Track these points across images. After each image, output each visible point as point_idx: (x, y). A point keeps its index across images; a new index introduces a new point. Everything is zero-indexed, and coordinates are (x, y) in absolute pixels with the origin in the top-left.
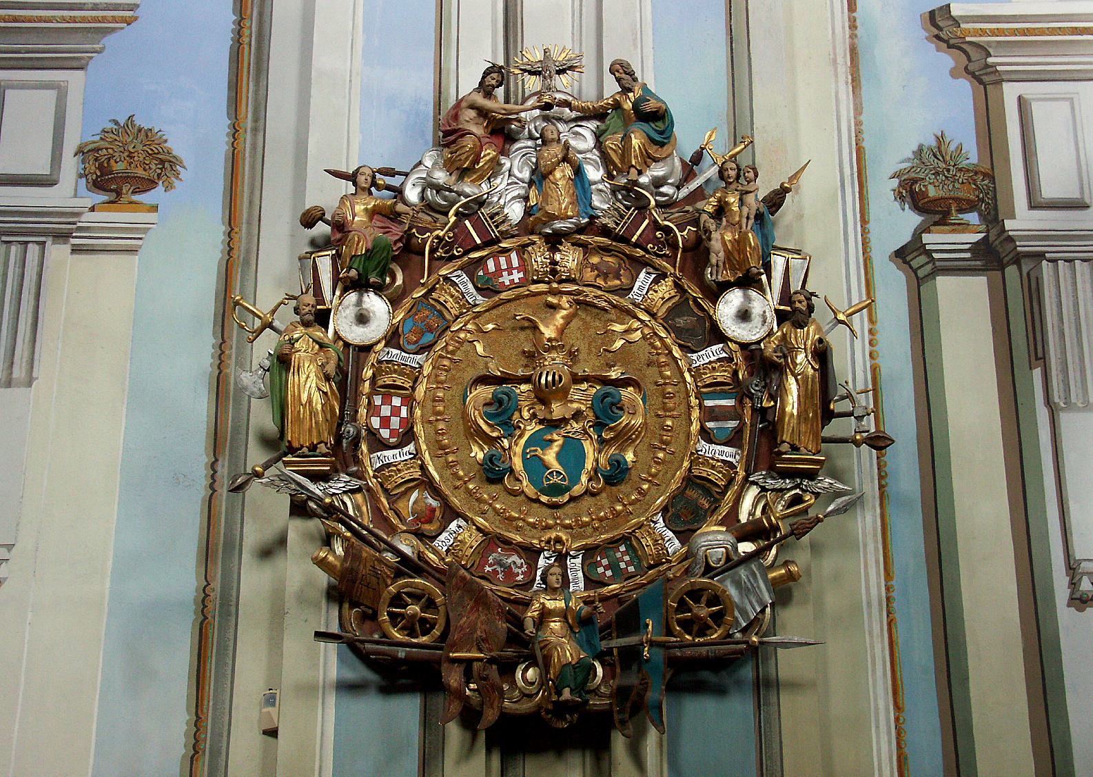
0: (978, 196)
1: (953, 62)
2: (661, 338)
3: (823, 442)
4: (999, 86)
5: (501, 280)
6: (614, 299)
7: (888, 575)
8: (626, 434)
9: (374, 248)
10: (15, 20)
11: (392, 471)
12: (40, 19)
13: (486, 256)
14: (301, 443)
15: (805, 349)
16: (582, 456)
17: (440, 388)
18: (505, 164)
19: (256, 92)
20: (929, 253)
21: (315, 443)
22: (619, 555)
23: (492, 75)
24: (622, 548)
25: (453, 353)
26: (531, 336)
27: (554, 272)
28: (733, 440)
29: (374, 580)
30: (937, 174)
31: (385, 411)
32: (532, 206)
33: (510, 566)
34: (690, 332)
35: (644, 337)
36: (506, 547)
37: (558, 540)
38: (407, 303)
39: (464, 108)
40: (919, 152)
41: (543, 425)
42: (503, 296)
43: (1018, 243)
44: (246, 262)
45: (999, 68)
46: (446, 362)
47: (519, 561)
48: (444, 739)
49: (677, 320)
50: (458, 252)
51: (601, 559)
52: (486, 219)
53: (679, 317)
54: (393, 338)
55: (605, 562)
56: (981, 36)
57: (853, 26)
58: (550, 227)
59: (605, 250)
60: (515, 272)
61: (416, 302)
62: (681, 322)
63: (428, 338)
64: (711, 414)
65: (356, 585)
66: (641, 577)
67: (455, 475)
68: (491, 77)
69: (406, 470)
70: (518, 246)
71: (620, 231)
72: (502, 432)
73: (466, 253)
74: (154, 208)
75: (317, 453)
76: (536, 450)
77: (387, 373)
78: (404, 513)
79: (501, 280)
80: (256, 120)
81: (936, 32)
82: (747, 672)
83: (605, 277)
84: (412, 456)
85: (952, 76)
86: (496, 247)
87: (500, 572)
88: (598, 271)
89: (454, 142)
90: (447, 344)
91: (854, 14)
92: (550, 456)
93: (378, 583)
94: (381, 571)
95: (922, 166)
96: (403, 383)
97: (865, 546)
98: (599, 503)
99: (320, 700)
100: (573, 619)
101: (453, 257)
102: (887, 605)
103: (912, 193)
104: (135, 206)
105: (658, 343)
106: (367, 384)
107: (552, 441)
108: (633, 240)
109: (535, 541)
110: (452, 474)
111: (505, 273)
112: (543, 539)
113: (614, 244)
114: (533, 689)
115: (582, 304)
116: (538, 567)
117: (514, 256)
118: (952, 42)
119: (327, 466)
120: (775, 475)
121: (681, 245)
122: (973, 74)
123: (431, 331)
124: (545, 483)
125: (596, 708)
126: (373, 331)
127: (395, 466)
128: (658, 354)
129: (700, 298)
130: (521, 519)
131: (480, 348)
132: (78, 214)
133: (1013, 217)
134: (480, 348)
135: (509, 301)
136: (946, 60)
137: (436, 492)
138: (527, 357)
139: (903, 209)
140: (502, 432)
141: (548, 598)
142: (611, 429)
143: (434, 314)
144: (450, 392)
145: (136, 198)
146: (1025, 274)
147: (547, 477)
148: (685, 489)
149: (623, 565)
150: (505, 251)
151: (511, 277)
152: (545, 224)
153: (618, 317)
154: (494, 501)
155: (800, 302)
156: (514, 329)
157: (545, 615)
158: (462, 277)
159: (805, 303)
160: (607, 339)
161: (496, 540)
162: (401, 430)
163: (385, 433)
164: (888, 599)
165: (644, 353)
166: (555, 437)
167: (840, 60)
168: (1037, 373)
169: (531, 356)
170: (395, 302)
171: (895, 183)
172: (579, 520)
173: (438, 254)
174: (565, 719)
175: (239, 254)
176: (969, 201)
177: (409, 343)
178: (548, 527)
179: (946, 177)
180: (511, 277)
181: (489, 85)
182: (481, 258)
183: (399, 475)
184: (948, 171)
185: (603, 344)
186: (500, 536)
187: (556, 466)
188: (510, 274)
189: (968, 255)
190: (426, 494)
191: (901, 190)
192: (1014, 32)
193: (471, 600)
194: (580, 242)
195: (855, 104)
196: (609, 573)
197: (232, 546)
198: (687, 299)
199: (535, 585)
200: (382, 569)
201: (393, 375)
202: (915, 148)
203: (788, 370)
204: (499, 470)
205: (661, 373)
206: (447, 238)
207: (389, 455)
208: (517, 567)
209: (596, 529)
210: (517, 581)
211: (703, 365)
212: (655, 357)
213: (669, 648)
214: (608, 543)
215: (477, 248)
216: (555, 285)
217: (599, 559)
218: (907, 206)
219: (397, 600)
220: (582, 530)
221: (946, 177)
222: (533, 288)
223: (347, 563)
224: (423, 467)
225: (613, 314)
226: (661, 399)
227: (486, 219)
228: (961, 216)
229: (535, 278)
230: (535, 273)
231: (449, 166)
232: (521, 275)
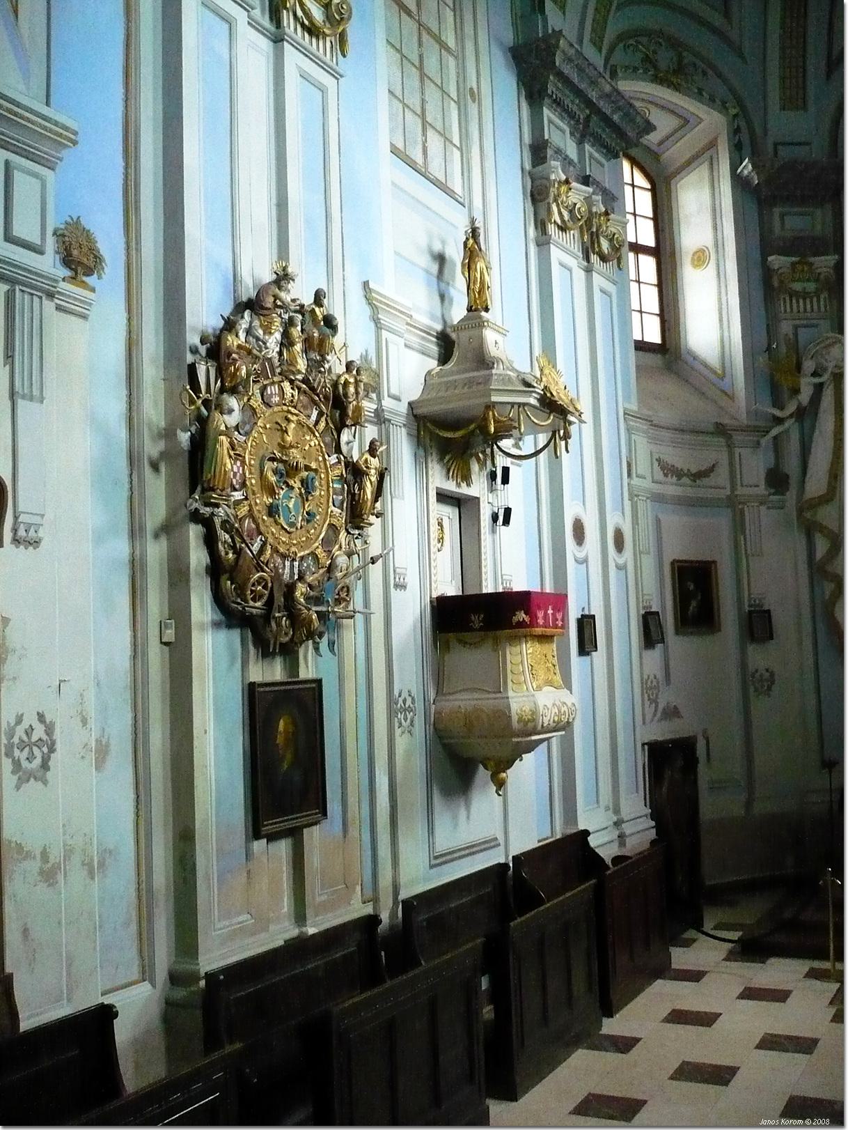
2: (321, 447)
4: (547, 246)
10: (16, 114)
12: (28, 120)
18: (231, 411)
44: (137, 344)
45: (382, 322)
74: (93, 290)
80: (137, 244)
97: (239, 923)
104: (85, 285)
132: (56, 281)
145: (85, 279)
152: (294, 373)
168: (563, 443)
175: (135, 329)
189: (373, 415)
197: (142, 528)
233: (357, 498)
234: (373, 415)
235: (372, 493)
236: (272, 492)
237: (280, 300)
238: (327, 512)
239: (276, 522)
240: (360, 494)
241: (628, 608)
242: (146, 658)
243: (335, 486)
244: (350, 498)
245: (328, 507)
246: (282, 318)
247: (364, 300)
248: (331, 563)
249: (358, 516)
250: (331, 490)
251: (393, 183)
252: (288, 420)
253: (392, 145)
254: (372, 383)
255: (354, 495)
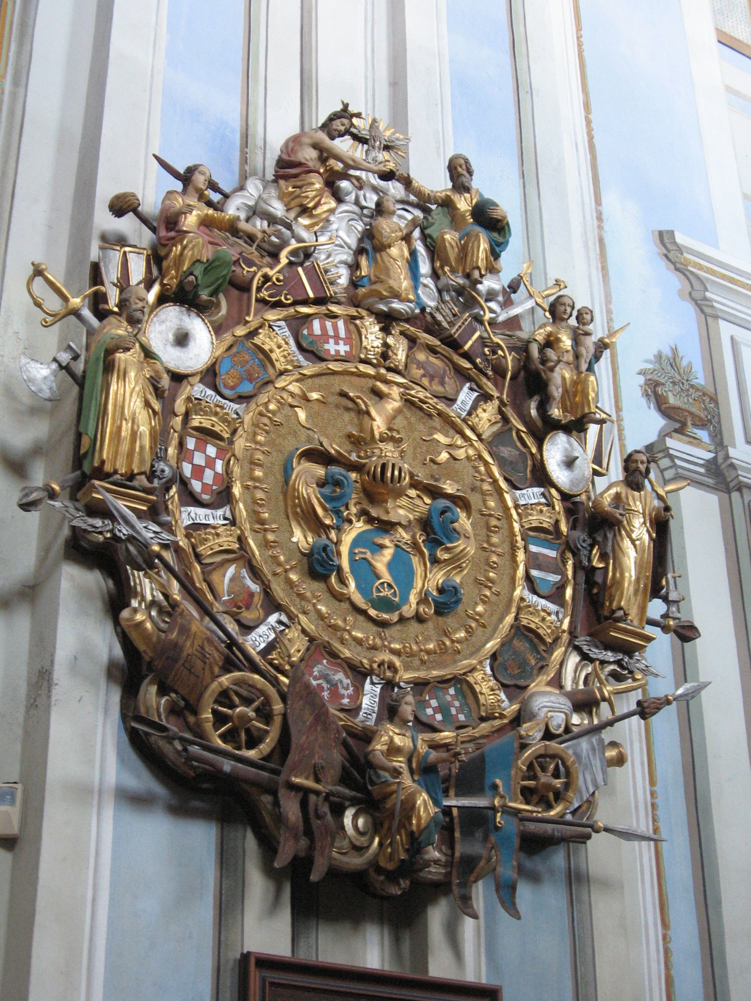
0: (707, 417)
1: (679, 284)
2: (486, 463)
5: (326, 346)
6: (441, 406)
8: (459, 559)
9: (214, 261)
11: (210, 533)
13: (312, 315)
14: (117, 467)
15: (644, 514)
17: (258, 449)
20: (672, 457)
21: (136, 471)
22: (449, 698)
23: (343, 120)
24: (452, 691)
25: (274, 413)
27: (385, 356)
29: (199, 664)
30: (674, 383)
31: (199, 459)
32: (364, 277)
33: (336, 685)
34: (513, 465)
35: (468, 458)
36: (332, 660)
37: (392, 667)
38: (228, 338)
39: (306, 144)
40: (659, 357)
42: (333, 366)
43: (740, 473)
45: (715, 304)
47: (347, 681)
48: (243, 886)
49: (501, 448)
50: (287, 299)
51: (430, 699)
52: (321, 272)
53: (503, 446)
54: (210, 375)
56: (699, 269)
57: (600, 218)
58: (386, 304)
60: (341, 342)
61: (237, 340)
63: (247, 388)
64: (533, 561)
66: (473, 729)
67: (275, 558)
68: (341, 122)
69: (226, 537)
70: (346, 315)
71: (455, 333)
72: (335, 521)
73: (295, 303)
75: (135, 483)
76: (365, 553)
77: (206, 413)
78: (219, 588)
79: (326, 346)
81: (665, 252)
82: (558, 858)
84: (227, 522)
85: (680, 296)
86: (324, 308)
87: (326, 688)
88: (424, 369)
90: (269, 401)
91: (600, 208)
92: (382, 562)
94: (209, 654)
95: (662, 371)
96: (221, 431)
98: (426, 633)
99: (95, 809)
100: (419, 763)
102: (652, 812)
103: (655, 393)
105: (482, 469)
106: (179, 420)
107: (382, 547)
108: (466, 347)
109: (365, 661)
110: (271, 556)
111: (332, 341)
112: (376, 659)
113: (443, 346)
116: (365, 693)
120: (599, 644)
121: (510, 368)
122: (695, 301)
123: (251, 380)
124: (375, 594)
125: (430, 876)
126: (191, 359)
128: (482, 480)
129: (523, 432)
130: (347, 630)
131: (302, 415)
133: (734, 447)
134: (302, 415)
135: (334, 373)
136: (675, 281)
137: (255, 573)
138: (352, 443)
139: (649, 408)
140: (335, 521)
141: (397, 731)
142: (448, 550)
143: (254, 362)
146: (746, 504)
147: (377, 587)
148: (513, 638)
149: (453, 711)
150: (333, 316)
151: (337, 347)
152: (382, 298)
154: (318, 601)
155: (642, 462)
157: (393, 750)
158: (284, 330)
159: (645, 465)
160: (432, 449)
161: (322, 649)
162: (214, 487)
164: (653, 805)
166: (387, 542)
167: (591, 245)
169: (356, 442)
170: (218, 329)
171: (641, 380)
173: (262, 295)
174: (399, 884)
177: (225, 386)
178: (374, 648)
179: (682, 389)
180: (337, 347)
181: (336, 130)
182: (308, 316)
183: (217, 541)
184: (683, 384)
185: (428, 452)
186: (327, 645)
187: (387, 577)
188: (337, 343)
189: (702, 470)
190: (244, 572)
191: (647, 389)
192: (724, 277)
193: (311, 715)
194: (408, 333)
195: (605, 292)
196: (439, 717)
198: (510, 430)
199: (361, 714)
200: (211, 652)
201: (214, 419)
202: (656, 353)
203: (623, 532)
205: (484, 501)
207: (200, 514)
208: (343, 688)
209: (423, 662)
210: (341, 704)
211: (531, 505)
213: (522, 820)
214: (438, 682)
215: (306, 302)
216: (383, 371)
217: (427, 698)
218: (652, 406)
219: (224, 697)
220: (409, 659)
221: (682, 389)
222: (363, 368)
223: (172, 634)
224: (241, 539)
225: (437, 422)
226: (485, 530)
227: (321, 272)
228: (696, 431)
229: (362, 356)
230: (364, 351)
231: (288, 200)
232: (347, 348)
233: (599, 579)
234: (702, 470)
235: (639, 566)
237: (338, 158)
238: (510, 600)
240: (606, 569)
241: (267, 14)
242: (22, 91)
243: (533, 548)
245: (514, 589)
246: (363, 208)
247: (663, 263)
248: (519, 711)
249: (607, 618)
251: (729, 89)
253: (719, 32)
254: (693, 410)
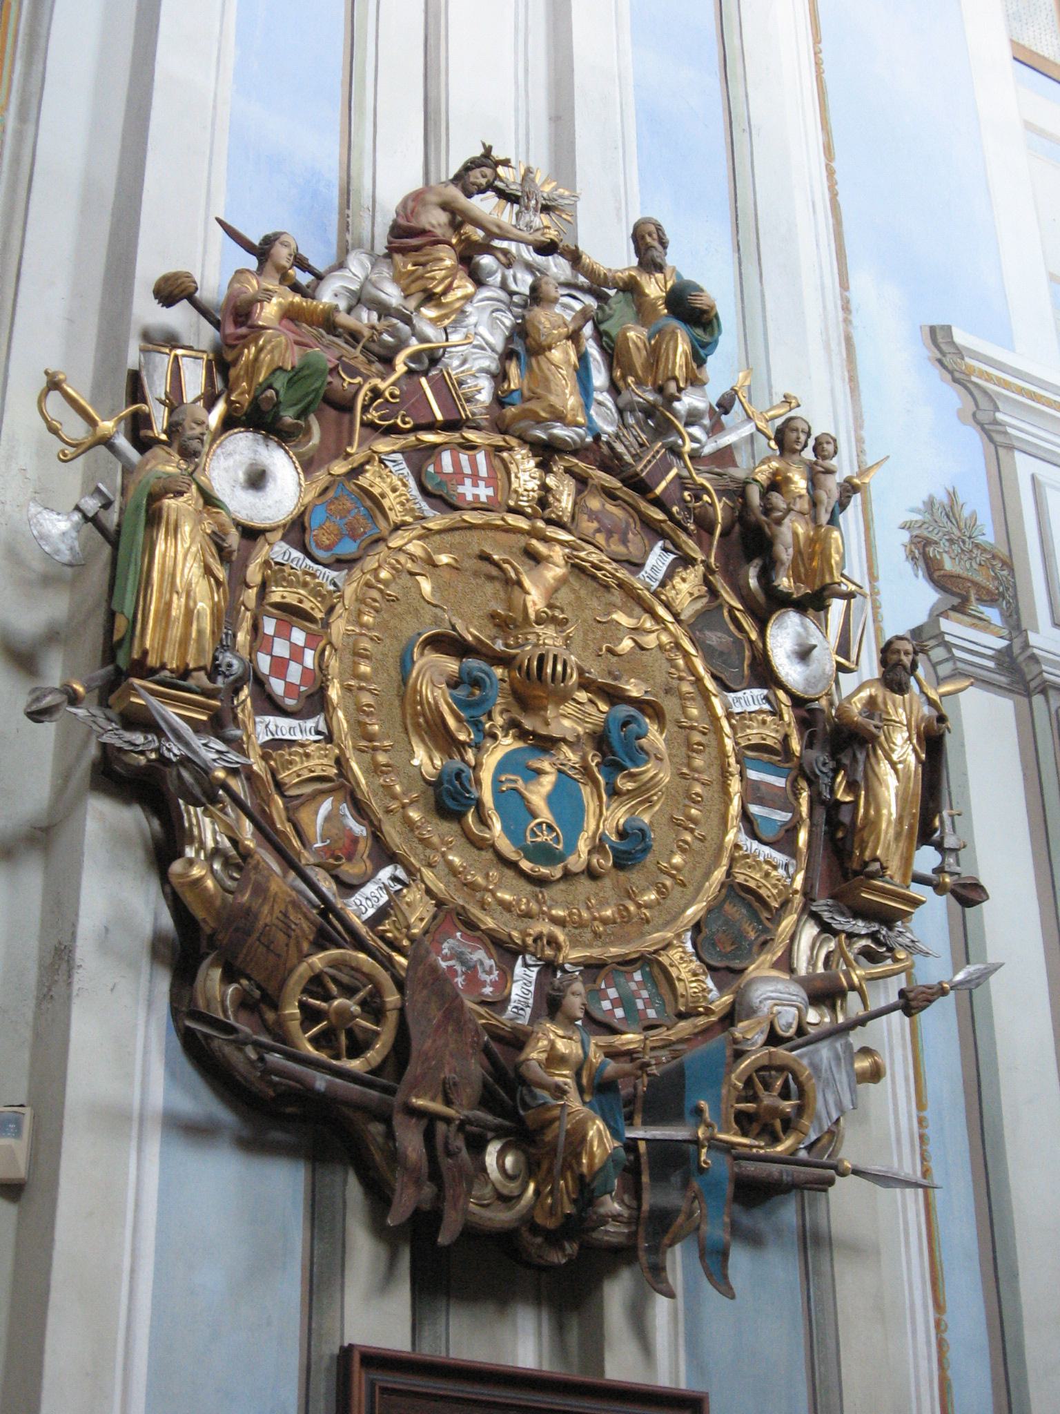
0: (997, 589)
1: (959, 401)
2: (686, 655)
3: (914, 881)
5: (461, 489)
6: (623, 574)
7: (921, 1106)
8: (648, 790)
9: (301, 369)
11: (297, 753)
13: (440, 444)
14: (165, 660)
16: (580, 810)
17: (365, 635)
19: (27, 75)
20: (948, 646)
21: (191, 666)
22: (633, 986)
23: (484, 169)
24: (638, 976)
25: (386, 583)
26: (502, 595)
28: (785, 841)
29: (281, 937)
30: (951, 541)
31: (281, 649)
32: (513, 391)
33: (475, 967)
34: (725, 657)
35: (661, 647)
36: (469, 932)
37: (553, 942)
39: (432, 204)
40: (930, 504)
41: (525, 742)
42: (470, 517)
43: (1044, 668)
45: (1009, 430)
46: (376, 594)
47: (489, 962)
48: (344, 1252)
50: (405, 423)
51: (607, 987)
52: (453, 384)
53: (710, 630)
54: (297, 530)
55: (613, 993)
56: (986, 380)
57: (846, 308)
58: (545, 429)
59: (610, 494)
60: (482, 484)
61: (334, 481)
62: (714, 638)
63: (348, 548)
64: (753, 792)
65: (250, 941)
66: (668, 1029)
67: (388, 788)
68: (481, 172)
69: (319, 758)
70: (489, 445)
71: (642, 470)
72: (472, 737)
73: (417, 428)
76: (515, 781)
77: (290, 584)
78: (308, 831)
79: (461, 489)
81: (939, 356)
83: (609, 534)
84: (321, 737)
85: (959, 418)
86: (457, 435)
87: (460, 972)
88: (599, 522)
89: (417, 249)
90: (380, 566)
91: (847, 294)
92: (539, 794)
93: (287, 945)
94: (296, 924)
95: (934, 524)
96: (312, 609)
98: (601, 894)
99: (134, 1143)
100: (591, 1078)
101: (393, 430)
102: (921, 1147)
103: (925, 556)
105: (681, 662)
107: (539, 772)
108: (658, 490)
109: (515, 934)
110: (383, 786)
113: (625, 489)
114: (511, 1188)
115: (577, 568)
116: (515, 978)
117: (481, 457)
118: (957, 375)
119: (202, 713)
121: (720, 520)
123: (354, 537)
124: (529, 839)
125: (606, 1238)
126: (269, 507)
127: (303, 745)
128: (681, 679)
129: (738, 610)
130: (490, 891)
131: (426, 586)
133: (1036, 631)
134: (426, 586)
135: (472, 527)
136: (953, 397)
137: (360, 809)
138: (496, 625)
139: (917, 576)
140: (472, 737)
141: (560, 1032)
142: (632, 776)
143: (359, 511)
144: (380, 647)
146: (1053, 712)
147: (532, 830)
148: (724, 901)
150: (470, 447)
151: (476, 491)
152: (539, 421)
153: (624, 603)
156: (476, 574)
158: (401, 466)
159: (911, 657)
161: (455, 917)
162: (303, 689)
163: (277, 686)
164: (922, 1137)
165: (659, 666)
166: (546, 765)
167: (834, 345)
169: (503, 624)
171: (905, 536)
172: (574, 914)
173: (369, 416)
174: (563, 1249)
176: (989, 592)
177: (318, 545)
180: (476, 491)
181: (474, 184)
182: (435, 446)
183: (306, 764)
185: (604, 639)
186: (461, 911)
187: (546, 815)
188: (475, 485)
189: (991, 664)
192: (1021, 391)
193: (439, 1010)
194: (576, 470)
195: (854, 412)
196: (619, 1013)
198: (720, 607)
199: (510, 1008)
201: (302, 592)
202: (925, 498)
204: (469, 798)
205: (684, 708)
206: (387, 394)
208: (484, 971)
209: (597, 935)
210: (482, 995)
211: (750, 713)
212: (675, 683)
213: (737, 1158)
214: (619, 964)
215: (431, 427)
216: (540, 524)
217: (603, 986)
218: (920, 573)
219: (316, 985)
220: (577, 931)
222: (512, 519)
224: (340, 762)
225: (617, 596)
227: (453, 384)
228: (982, 608)
229: (512, 503)
230: (514, 496)
232: (490, 492)
233: (845, 817)
234: (991, 664)
235: (902, 799)
236: (443, 740)
237: (478, 224)
238: (721, 847)
239: (478, 844)
240: (855, 804)
241: (377, 20)
243: (753, 775)
244: (821, 815)
247: (935, 372)
248: (733, 1004)
249: (856, 873)
250: (735, 786)
251: (1028, 126)
252: (535, 558)
253: (1015, 45)
254: (979, 579)
255: (834, 807)
